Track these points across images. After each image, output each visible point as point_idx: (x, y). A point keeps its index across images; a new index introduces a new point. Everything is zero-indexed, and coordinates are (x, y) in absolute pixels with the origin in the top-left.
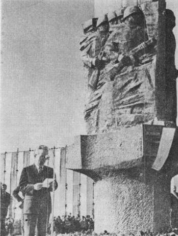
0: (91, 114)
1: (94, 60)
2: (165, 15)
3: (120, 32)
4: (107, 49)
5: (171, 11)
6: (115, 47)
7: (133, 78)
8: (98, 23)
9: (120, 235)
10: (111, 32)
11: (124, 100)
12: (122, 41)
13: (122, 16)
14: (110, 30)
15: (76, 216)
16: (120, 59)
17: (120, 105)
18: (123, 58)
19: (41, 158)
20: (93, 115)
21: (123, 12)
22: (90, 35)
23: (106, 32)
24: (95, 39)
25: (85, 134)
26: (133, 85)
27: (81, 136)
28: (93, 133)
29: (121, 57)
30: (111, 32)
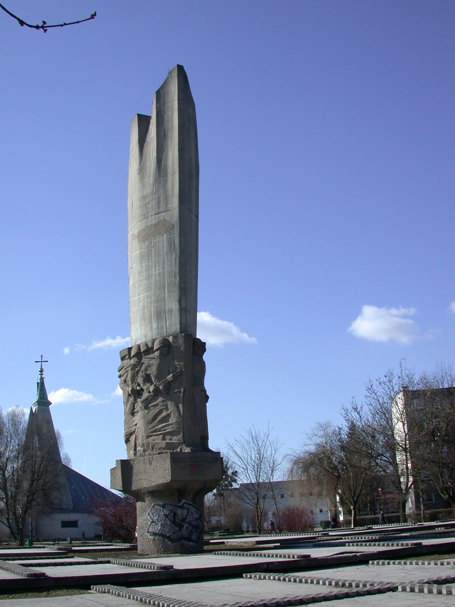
0: (200, 335)
2: (153, 391)
3: (152, 362)
4: (140, 380)
5: (207, 398)
6: (147, 379)
7: (164, 407)
10: (143, 363)
11: (157, 427)
12: (153, 371)
16: (151, 390)
17: (155, 431)
20: (133, 438)
21: (153, 343)
22: (127, 362)
23: (139, 363)
24: (130, 368)
26: (164, 414)
27: (121, 460)
28: (133, 457)
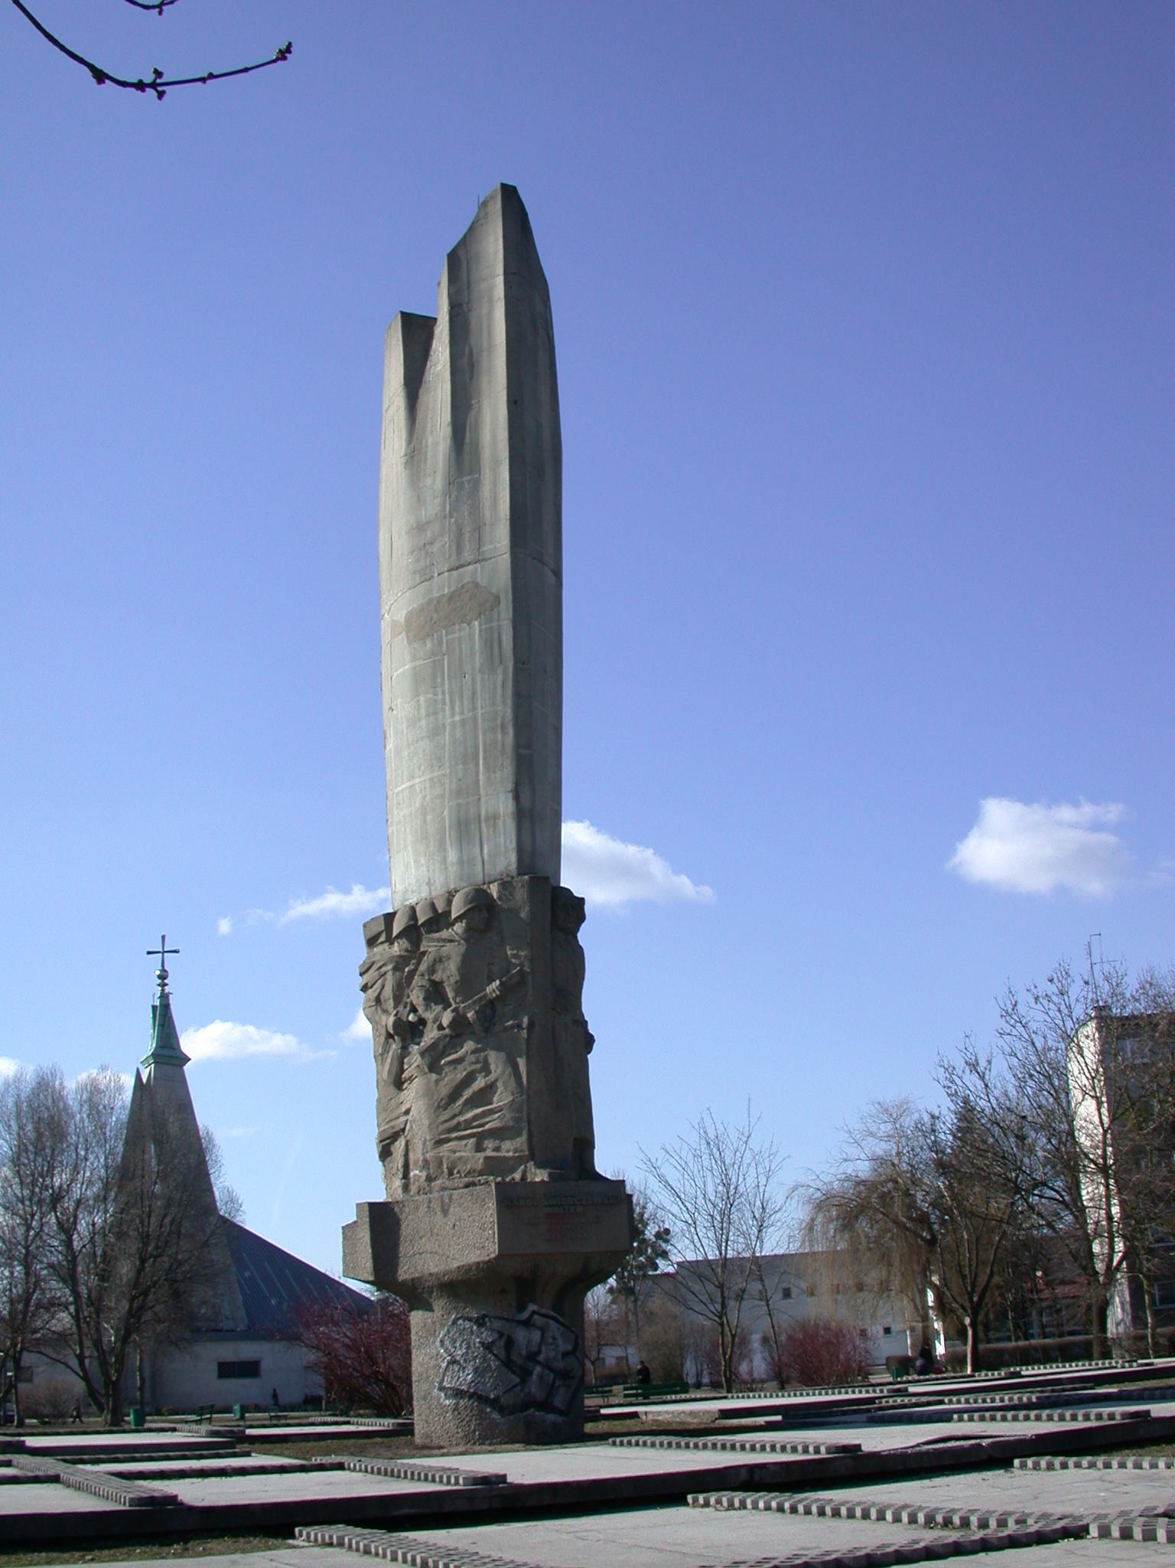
1: (391, 1019)
3: (447, 951)
4: (416, 996)
6: (435, 994)
8: (397, 929)
9: (1017, 1462)
10: (424, 953)
12: (449, 973)
13: (448, 913)
14: (422, 949)
15: (625, 1368)
18: (454, 1019)
19: (383, 1115)
20: (399, 1147)
21: (449, 902)
22: (382, 950)
25: (381, 1197)
26: (480, 1083)
27: (370, 1204)
28: (399, 1194)
29: (447, 1018)
30: (424, 953)
